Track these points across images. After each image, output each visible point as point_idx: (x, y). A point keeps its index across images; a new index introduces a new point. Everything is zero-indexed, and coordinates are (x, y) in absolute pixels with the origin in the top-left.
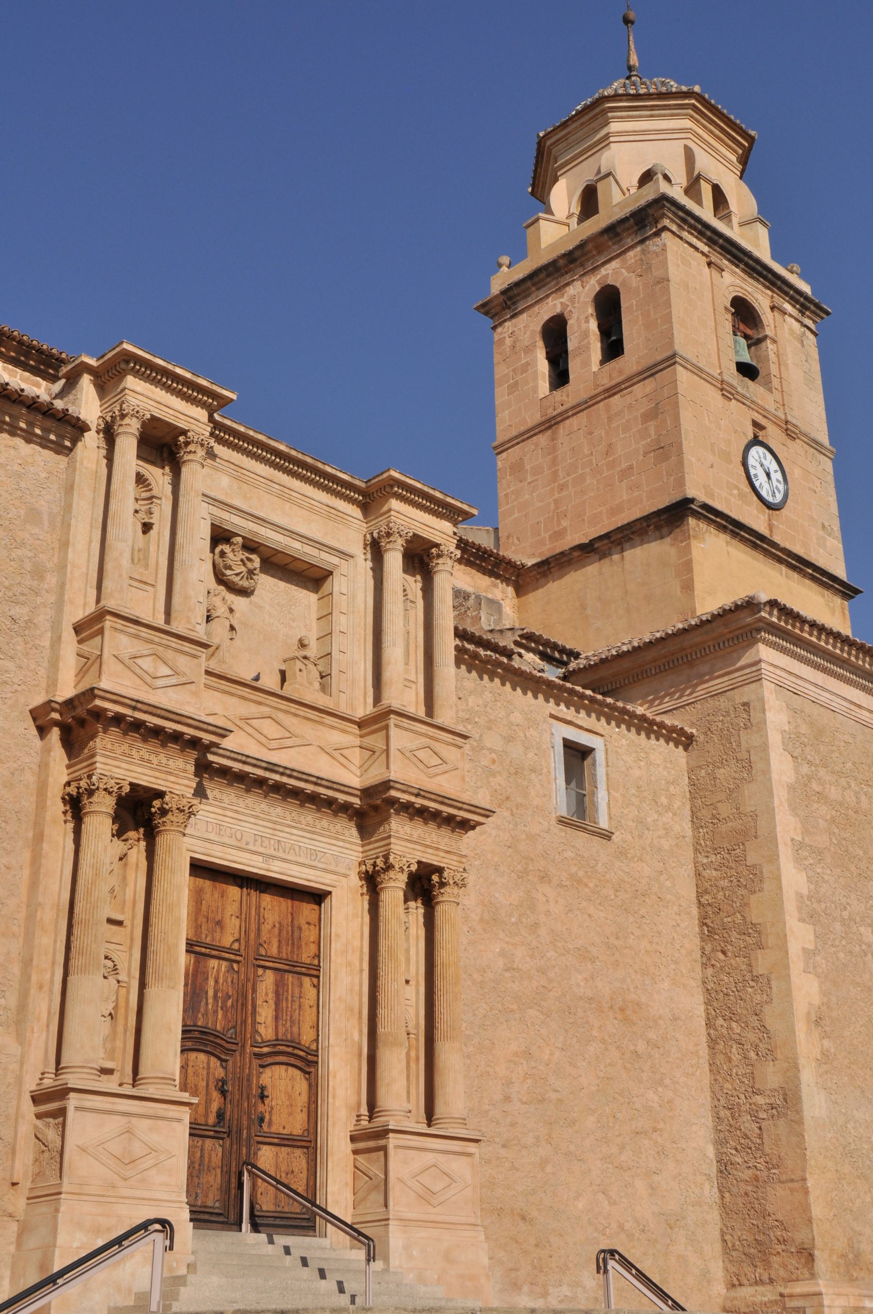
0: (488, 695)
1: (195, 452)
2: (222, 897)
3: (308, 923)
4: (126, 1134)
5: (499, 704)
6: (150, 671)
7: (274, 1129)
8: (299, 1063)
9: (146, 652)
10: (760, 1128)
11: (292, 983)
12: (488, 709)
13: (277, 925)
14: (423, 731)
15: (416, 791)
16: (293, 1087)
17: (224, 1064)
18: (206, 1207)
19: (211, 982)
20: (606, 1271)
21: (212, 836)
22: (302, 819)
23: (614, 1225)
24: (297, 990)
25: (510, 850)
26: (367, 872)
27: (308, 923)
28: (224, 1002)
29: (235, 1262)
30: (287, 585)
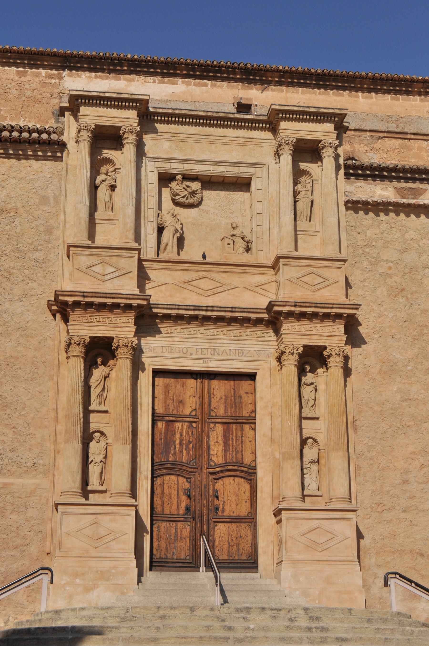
0: (384, 226)
1: (127, 138)
2: (183, 386)
3: (247, 393)
4: (95, 525)
5: (394, 229)
6: (101, 272)
7: (226, 514)
8: (243, 475)
9: (97, 262)
11: (236, 429)
12: (385, 235)
13: (223, 397)
14: (307, 264)
15: (293, 304)
16: (239, 489)
17: (189, 480)
18: (180, 559)
19: (178, 436)
21: (166, 355)
22: (231, 333)
25: (406, 323)
27: (247, 393)
28: (187, 445)
29: (171, 588)
30: (226, 192)
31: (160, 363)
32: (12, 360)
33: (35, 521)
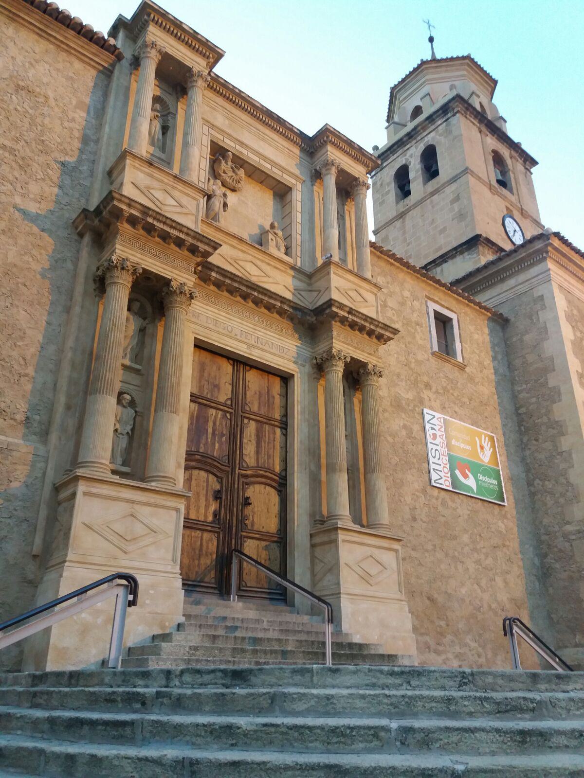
2: (219, 370)
10: (571, 545)
13: (258, 393)
19: (211, 424)
20: (512, 634)
21: (211, 326)
23: (485, 606)
24: (272, 436)
26: (317, 363)
31: (204, 334)
32: (14, 270)
33: (20, 503)
